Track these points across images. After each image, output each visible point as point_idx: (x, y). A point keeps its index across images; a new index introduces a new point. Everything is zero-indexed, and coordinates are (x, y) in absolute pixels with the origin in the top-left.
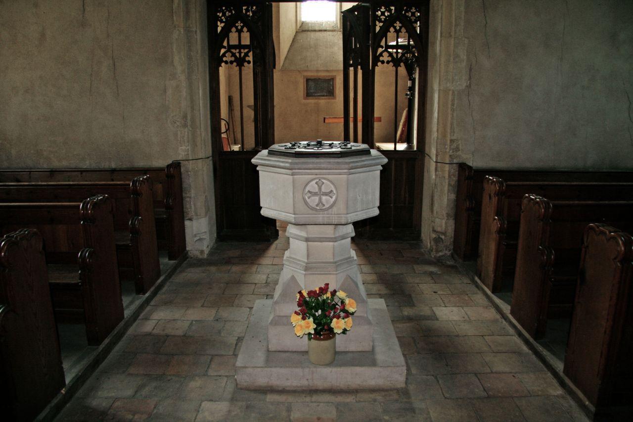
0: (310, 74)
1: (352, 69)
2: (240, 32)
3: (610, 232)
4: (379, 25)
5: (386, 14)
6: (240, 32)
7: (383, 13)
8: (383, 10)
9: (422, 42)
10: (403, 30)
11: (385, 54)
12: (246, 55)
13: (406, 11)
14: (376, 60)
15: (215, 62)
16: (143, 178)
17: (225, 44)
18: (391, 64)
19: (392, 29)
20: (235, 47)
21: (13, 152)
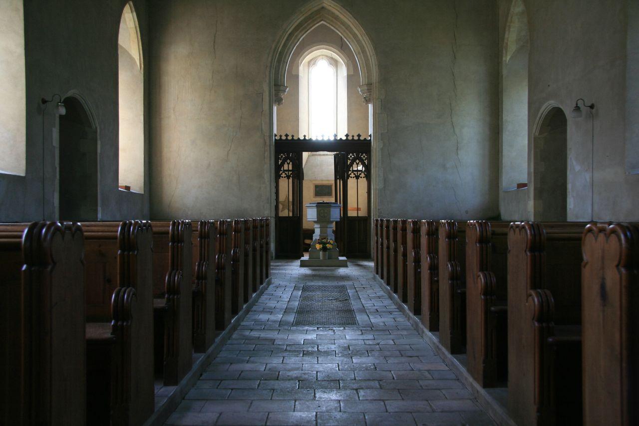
0: (317, 183)
1: (338, 181)
2: (288, 164)
3: (331, 239)
4: (349, 162)
5: (353, 157)
6: (288, 164)
7: (351, 157)
8: (366, 157)
9: (368, 168)
10: (360, 163)
11: (284, 174)
12: (360, 174)
13: (361, 155)
14: (348, 176)
15: (278, 177)
16: (141, 222)
17: (282, 169)
18: (355, 178)
19: (286, 163)
20: (286, 171)
21: (189, 213)
